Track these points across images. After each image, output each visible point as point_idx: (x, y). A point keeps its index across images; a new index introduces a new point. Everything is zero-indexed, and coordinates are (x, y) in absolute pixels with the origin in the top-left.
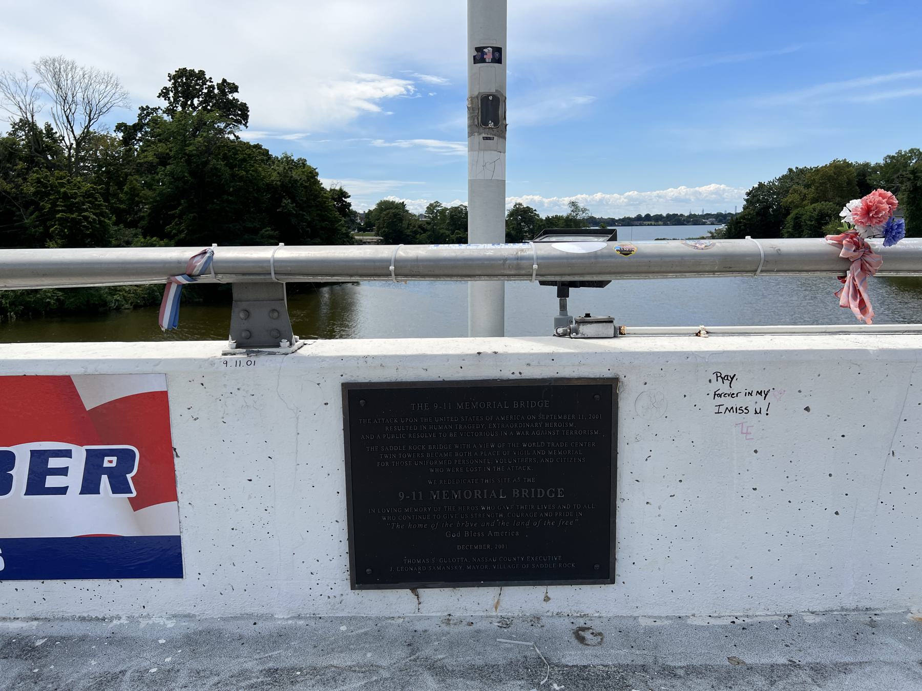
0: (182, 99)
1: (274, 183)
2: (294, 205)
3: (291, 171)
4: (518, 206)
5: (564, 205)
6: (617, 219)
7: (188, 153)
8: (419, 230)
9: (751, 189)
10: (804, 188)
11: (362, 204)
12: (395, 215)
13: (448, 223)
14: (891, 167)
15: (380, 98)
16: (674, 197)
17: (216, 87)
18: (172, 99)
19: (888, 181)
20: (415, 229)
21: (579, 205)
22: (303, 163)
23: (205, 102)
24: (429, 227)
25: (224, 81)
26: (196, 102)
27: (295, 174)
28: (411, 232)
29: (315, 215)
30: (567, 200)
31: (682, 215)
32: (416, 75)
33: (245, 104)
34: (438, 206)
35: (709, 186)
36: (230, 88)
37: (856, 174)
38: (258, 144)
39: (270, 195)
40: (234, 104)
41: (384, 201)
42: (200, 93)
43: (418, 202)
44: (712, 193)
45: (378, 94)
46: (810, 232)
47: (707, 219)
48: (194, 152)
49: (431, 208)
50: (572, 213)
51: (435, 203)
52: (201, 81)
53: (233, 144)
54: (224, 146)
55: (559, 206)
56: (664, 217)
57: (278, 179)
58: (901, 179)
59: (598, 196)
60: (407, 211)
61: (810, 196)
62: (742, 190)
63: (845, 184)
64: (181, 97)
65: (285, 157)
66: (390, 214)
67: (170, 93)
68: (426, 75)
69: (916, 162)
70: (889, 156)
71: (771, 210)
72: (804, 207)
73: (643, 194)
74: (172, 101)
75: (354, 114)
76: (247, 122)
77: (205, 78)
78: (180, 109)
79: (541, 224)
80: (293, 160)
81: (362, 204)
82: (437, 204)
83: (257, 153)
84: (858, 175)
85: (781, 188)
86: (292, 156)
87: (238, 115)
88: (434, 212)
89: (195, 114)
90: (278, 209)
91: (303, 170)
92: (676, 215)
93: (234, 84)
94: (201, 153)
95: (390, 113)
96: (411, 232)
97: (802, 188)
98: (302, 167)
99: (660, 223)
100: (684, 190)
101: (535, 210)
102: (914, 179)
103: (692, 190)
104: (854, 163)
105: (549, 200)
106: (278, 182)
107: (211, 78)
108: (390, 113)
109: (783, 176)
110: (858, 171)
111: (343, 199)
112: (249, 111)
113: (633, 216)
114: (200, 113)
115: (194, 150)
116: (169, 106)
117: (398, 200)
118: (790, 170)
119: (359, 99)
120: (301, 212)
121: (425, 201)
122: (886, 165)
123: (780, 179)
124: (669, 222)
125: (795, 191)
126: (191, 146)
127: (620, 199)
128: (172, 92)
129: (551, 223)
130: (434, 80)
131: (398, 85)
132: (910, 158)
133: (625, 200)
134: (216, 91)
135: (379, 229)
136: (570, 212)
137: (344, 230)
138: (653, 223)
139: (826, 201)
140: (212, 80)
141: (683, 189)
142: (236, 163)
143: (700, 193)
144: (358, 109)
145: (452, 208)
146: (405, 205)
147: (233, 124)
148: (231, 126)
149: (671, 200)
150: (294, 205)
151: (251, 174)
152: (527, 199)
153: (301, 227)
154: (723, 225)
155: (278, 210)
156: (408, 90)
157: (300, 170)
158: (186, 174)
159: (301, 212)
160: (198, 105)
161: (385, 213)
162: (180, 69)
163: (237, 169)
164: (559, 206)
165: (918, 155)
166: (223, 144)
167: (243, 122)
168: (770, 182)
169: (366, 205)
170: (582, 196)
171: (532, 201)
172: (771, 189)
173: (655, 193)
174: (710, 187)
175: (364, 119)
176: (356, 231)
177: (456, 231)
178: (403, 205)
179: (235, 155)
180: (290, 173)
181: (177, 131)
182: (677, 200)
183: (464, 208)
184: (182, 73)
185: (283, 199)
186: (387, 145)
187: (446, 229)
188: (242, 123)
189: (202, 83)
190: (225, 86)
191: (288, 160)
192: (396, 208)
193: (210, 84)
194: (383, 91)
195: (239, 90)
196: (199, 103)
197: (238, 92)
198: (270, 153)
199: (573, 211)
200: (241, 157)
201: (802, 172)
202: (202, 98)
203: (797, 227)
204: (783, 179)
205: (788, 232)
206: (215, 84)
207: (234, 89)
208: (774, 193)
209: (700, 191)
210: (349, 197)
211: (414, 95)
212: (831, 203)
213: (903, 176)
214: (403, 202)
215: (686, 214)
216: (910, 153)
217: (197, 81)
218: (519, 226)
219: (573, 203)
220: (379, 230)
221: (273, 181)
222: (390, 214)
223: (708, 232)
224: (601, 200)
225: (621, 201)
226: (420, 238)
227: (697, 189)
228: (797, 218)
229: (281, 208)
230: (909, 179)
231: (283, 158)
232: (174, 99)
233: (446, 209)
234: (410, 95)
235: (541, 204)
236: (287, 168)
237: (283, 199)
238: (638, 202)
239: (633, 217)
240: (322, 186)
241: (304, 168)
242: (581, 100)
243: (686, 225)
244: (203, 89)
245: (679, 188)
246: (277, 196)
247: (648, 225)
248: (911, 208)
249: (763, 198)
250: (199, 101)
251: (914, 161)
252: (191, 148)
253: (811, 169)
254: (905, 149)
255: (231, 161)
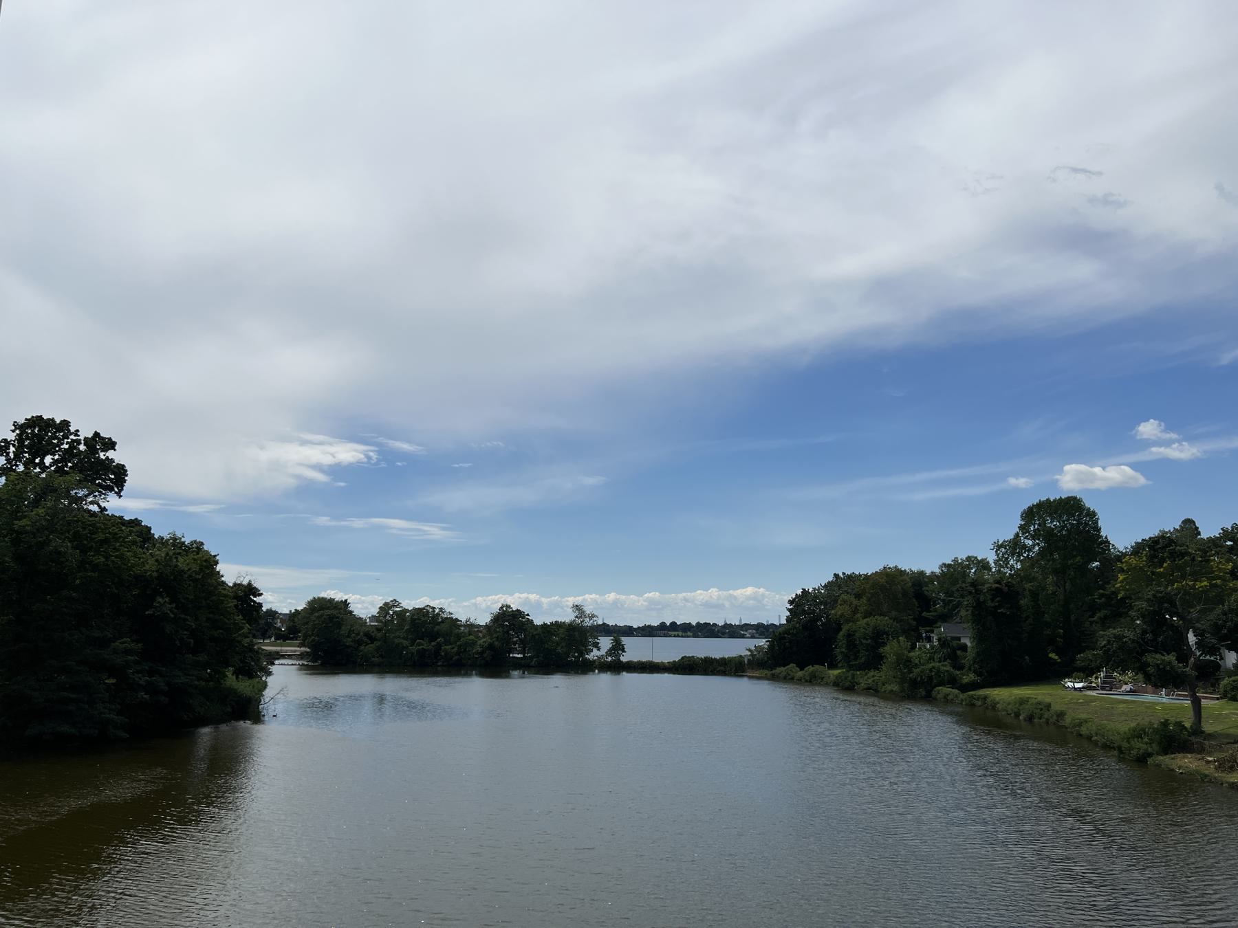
0: (27, 455)
1: (148, 574)
2: (174, 605)
3: (177, 558)
4: (505, 609)
5: (567, 606)
6: (635, 627)
7: (16, 529)
8: (365, 639)
9: (794, 597)
10: (855, 598)
11: (289, 601)
12: (331, 618)
13: (407, 629)
14: (948, 576)
15: (330, 466)
16: (704, 601)
17: (83, 442)
18: (12, 455)
19: (947, 593)
20: (359, 637)
21: (585, 609)
22: (197, 548)
23: (63, 460)
24: (379, 635)
25: (97, 434)
26: (48, 460)
27: (182, 563)
28: (352, 642)
29: (205, 619)
30: (571, 601)
31: (715, 625)
32: (381, 439)
33: (123, 466)
34: (396, 606)
35: (745, 590)
36: (103, 444)
37: (910, 584)
38: (136, 519)
39: (138, 591)
40: (108, 465)
41: (319, 598)
42: (57, 449)
43: (370, 598)
44: (749, 598)
45: (327, 460)
46: (867, 653)
47: (746, 631)
48: (29, 528)
49: (385, 608)
50: (577, 619)
51: (392, 601)
52: (62, 434)
53: (93, 519)
54: (78, 521)
55: (562, 608)
56: (693, 627)
57: (154, 568)
58: (961, 592)
59: (611, 597)
60: (351, 612)
61: (862, 609)
62: (784, 595)
63: (901, 595)
64: (26, 452)
65: (171, 538)
66: (325, 616)
67: (11, 447)
68: (395, 440)
69: (975, 571)
70: (944, 564)
71: (819, 623)
72: (855, 622)
73: (667, 596)
74: (12, 457)
75: (292, 482)
76: (122, 489)
77: (69, 430)
78: (21, 468)
79: (535, 633)
80: (184, 543)
81: (289, 601)
82: (395, 603)
83: (137, 531)
84: (914, 585)
85: (828, 596)
86: (183, 537)
87: (110, 479)
88: (389, 614)
89: (44, 476)
90: (148, 610)
91: (196, 557)
92: (707, 624)
93: (110, 439)
94: (38, 530)
95: (342, 484)
96: (352, 642)
97: (852, 598)
98: (195, 553)
99: (689, 633)
100: (716, 594)
101: (528, 615)
102: (976, 592)
103: (725, 593)
104: (908, 571)
105: (549, 600)
106: (155, 573)
107: (78, 431)
108: (342, 484)
109: (829, 583)
110: (913, 580)
111: (252, 597)
112: (127, 476)
113: (655, 623)
114: (50, 475)
115: (28, 525)
116: (5, 464)
117: (338, 596)
118: (836, 576)
119: (301, 464)
120: (183, 616)
121: (380, 598)
122: (943, 573)
123: (825, 586)
124: (700, 634)
125: (845, 602)
126: (25, 520)
127: (639, 601)
128: (14, 446)
129: (549, 632)
130: (406, 447)
131: (356, 451)
132: (968, 567)
133: (645, 603)
134: (82, 447)
135: (306, 636)
136: (573, 618)
137: (246, 641)
138: (680, 633)
139: (880, 615)
140: (79, 434)
141: (714, 592)
142: (92, 546)
143: (735, 598)
144: (299, 477)
145: (415, 609)
146: (349, 603)
147: (99, 492)
148: (97, 493)
149: (701, 605)
150: (174, 605)
151: (113, 561)
152: (520, 598)
153: (179, 637)
154: (764, 640)
155: (147, 613)
156: (369, 458)
157: (191, 556)
158: (7, 559)
159: (183, 616)
160: (50, 465)
161: (317, 614)
162: (33, 417)
163: (92, 553)
164: (562, 608)
165: (976, 564)
166: (75, 519)
167: (116, 490)
168: (815, 589)
169: (293, 602)
170: (591, 596)
171: (527, 601)
172: (816, 597)
173: (681, 596)
174: (747, 591)
175: (305, 490)
176: (273, 639)
177: (418, 641)
178: (345, 603)
179: (91, 534)
180: (175, 560)
181: (7, 499)
182: (708, 605)
183: (431, 610)
184: (36, 421)
185: (158, 597)
186: (333, 523)
187: (404, 638)
188: (113, 490)
189: (62, 436)
190: (96, 441)
191: (176, 544)
192: (335, 607)
193: (75, 438)
194: (334, 457)
195: (116, 448)
196: (52, 462)
197: (115, 450)
198: (152, 532)
199: (577, 617)
200: (101, 536)
201: (851, 578)
202: (59, 455)
203: (851, 647)
204: (828, 586)
205: (842, 652)
206: (82, 438)
207: (110, 445)
208: (821, 603)
209: (735, 594)
210: (261, 594)
211: (376, 464)
212: (886, 618)
213: (963, 588)
214: (346, 601)
215: (721, 623)
216: (968, 561)
217: (55, 432)
218: (506, 635)
219: (577, 606)
220: (306, 639)
221: (146, 571)
222: (325, 616)
223: (747, 649)
224: (615, 602)
225: (640, 603)
226: (366, 651)
227: (731, 592)
228: (849, 635)
229: (153, 609)
230: (970, 593)
231: (169, 540)
232: (15, 455)
233: (405, 611)
234: (370, 463)
235: (538, 605)
236: (171, 553)
237: (158, 597)
238: (660, 607)
239: (656, 625)
240: (223, 579)
241: (198, 554)
242: (590, 481)
243: (721, 637)
244: (62, 444)
245: (710, 591)
246: (148, 592)
247: (675, 636)
248: (977, 627)
249: (809, 608)
250: (53, 459)
251: (973, 571)
252: (24, 522)
253: (860, 575)
254: (962, 556)
255: (85, 542)
